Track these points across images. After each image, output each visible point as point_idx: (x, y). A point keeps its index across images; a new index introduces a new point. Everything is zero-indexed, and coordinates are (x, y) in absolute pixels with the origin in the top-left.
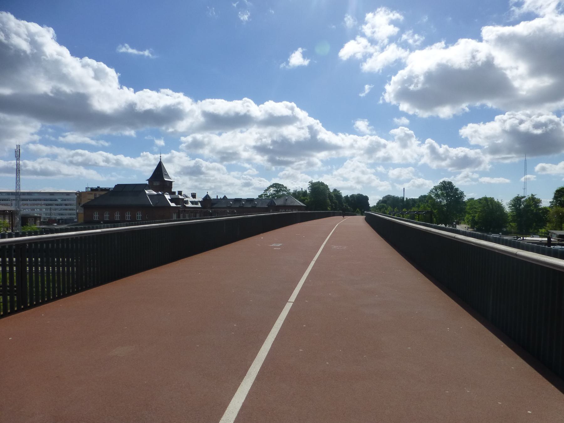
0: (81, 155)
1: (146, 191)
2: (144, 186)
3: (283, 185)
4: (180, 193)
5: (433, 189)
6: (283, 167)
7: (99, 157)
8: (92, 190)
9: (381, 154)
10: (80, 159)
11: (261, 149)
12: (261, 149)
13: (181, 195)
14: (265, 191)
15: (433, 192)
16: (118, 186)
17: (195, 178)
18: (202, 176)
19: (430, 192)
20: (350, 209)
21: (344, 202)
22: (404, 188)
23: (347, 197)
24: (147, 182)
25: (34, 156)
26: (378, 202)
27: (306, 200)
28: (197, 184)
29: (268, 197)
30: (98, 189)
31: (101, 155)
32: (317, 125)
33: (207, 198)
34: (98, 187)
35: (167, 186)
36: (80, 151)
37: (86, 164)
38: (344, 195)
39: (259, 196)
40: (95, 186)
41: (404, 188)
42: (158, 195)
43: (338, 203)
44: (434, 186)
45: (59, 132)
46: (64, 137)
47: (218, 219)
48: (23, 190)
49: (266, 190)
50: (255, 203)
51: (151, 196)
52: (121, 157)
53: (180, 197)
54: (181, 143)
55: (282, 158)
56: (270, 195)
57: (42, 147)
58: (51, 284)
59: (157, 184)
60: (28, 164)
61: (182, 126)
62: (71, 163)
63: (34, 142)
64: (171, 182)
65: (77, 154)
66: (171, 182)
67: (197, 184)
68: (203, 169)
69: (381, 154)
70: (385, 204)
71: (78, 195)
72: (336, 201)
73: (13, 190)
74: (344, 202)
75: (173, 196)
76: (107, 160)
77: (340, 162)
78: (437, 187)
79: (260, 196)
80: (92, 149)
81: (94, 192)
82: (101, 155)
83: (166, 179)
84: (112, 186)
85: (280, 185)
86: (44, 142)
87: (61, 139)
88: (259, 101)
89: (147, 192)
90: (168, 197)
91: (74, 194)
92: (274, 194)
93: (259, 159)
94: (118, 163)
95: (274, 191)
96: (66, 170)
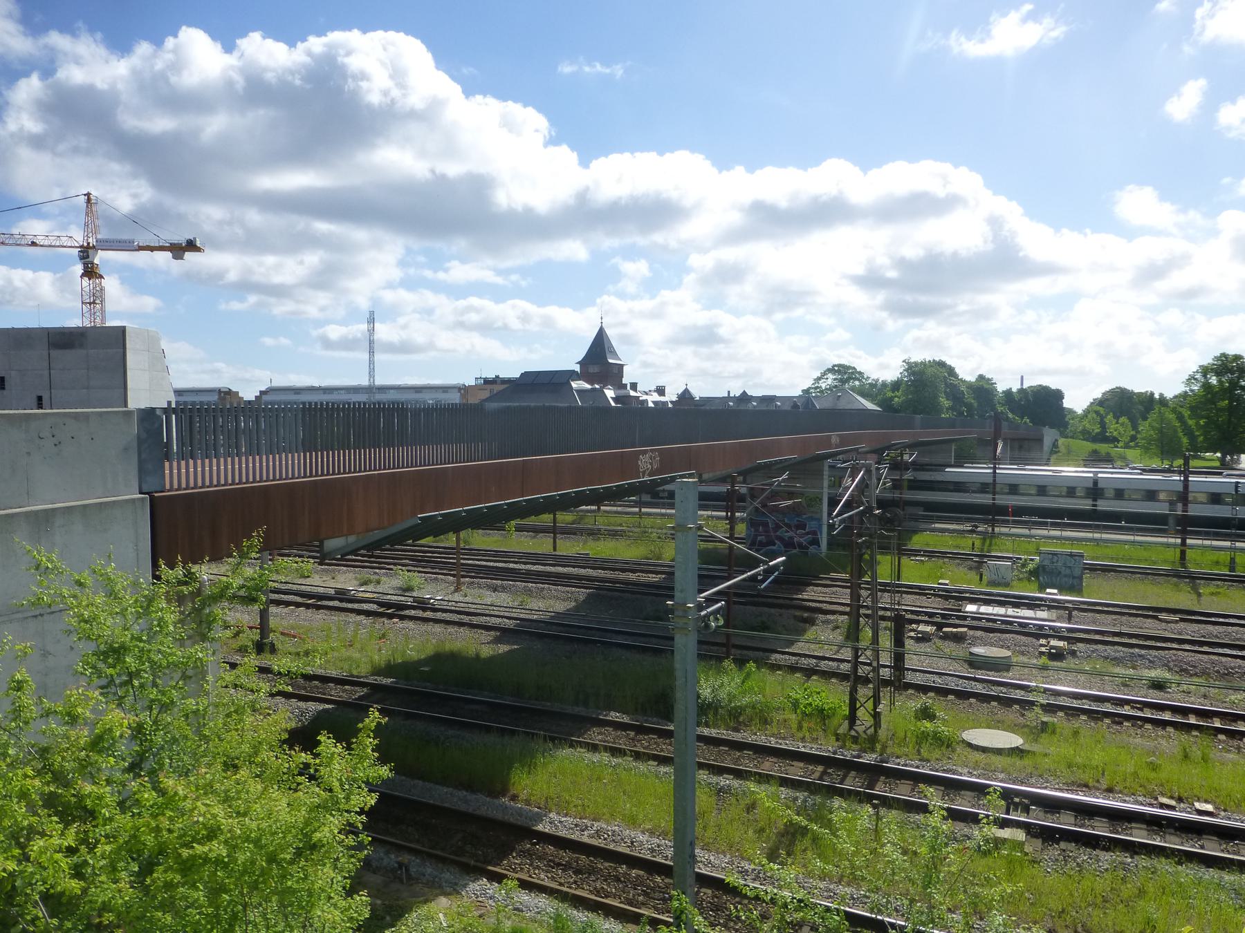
0: (477, 310)
1: (572, 383)
2: (571, 375)
3: (854, 368)
4: (634, 386)
5: (1197, 372)
6: (917, 321)
7: (509, 311)
8: (487, 381)
9: (1179, 280)
10: (474, 317)
11: (871, 281)
12: (871, 281)
13: (635, 390)
14: (815, 380)
15: (1195, 379)
16: (525, 375)
17: (704, 351)
18: (719, 348)
19: (1189, 379)
20: (1014, 418)
21: (999, 403)
22: (1022, 377)
23: (1008, 393)
24: (577, 368)
25: (393, 312)
26: (1092, 403)
27: (896, 399)
28: (707, 365)
29: (822, 392)
30: (496, 381)
31: (514, 307)
32: (1012, 213)
33: (685, 396)
34: (497, 377)
35: (613, 375)
36: (474, 301)
37: (485, 328)
38: (1001, 388)
39: (803, 391)
40: (491, 375)
41: (1022, 377)
42: (593, 390)
43: (976, 405)
44: (1200, 366)
45: (438, 262)
46: (446, 270)
47: (174, 430)
48: (379, 381)
49: (819, 379)
50: (776, 405)
51: (580, 392)
52: (552, 311)
53: (632, 393)
54: (688, 270)
55: (923, 299)
56: (826, 389)
57: (403, 295)
58: (175, 451)
59: (594, 369)
60: (383, 332)
61: (687, 230)
62: (461, 325)
63: (390, 286)
64: (621, 366)
65: (470, 309)
66: (621, 366)
67: (707, 365)
68: (722, 331)
69: (1179, 280)
70: (1101, 408)
71: (462, 391)
72: (973, 401)
73: (364, 382)
74: (999, 403)
75: (622, 392)
76: (525, 318)
77: (1064, 304)
78: (1206, 367)
79: (806, 391)
80: (497, 294)
81: (489, 387)
82: (514, 307)
83: (610, 361)
84: (515, 374)
85: (849, 367)
86: (409, 284)
87: (441, 275)
88: (867, 160)
89: (574, 385)
90: (610, 393)
91: (457, 390)
92: (836, 386)
93: (859, 299)
94: (548, 322)
95: (835, 379)
96: (445, 340)
